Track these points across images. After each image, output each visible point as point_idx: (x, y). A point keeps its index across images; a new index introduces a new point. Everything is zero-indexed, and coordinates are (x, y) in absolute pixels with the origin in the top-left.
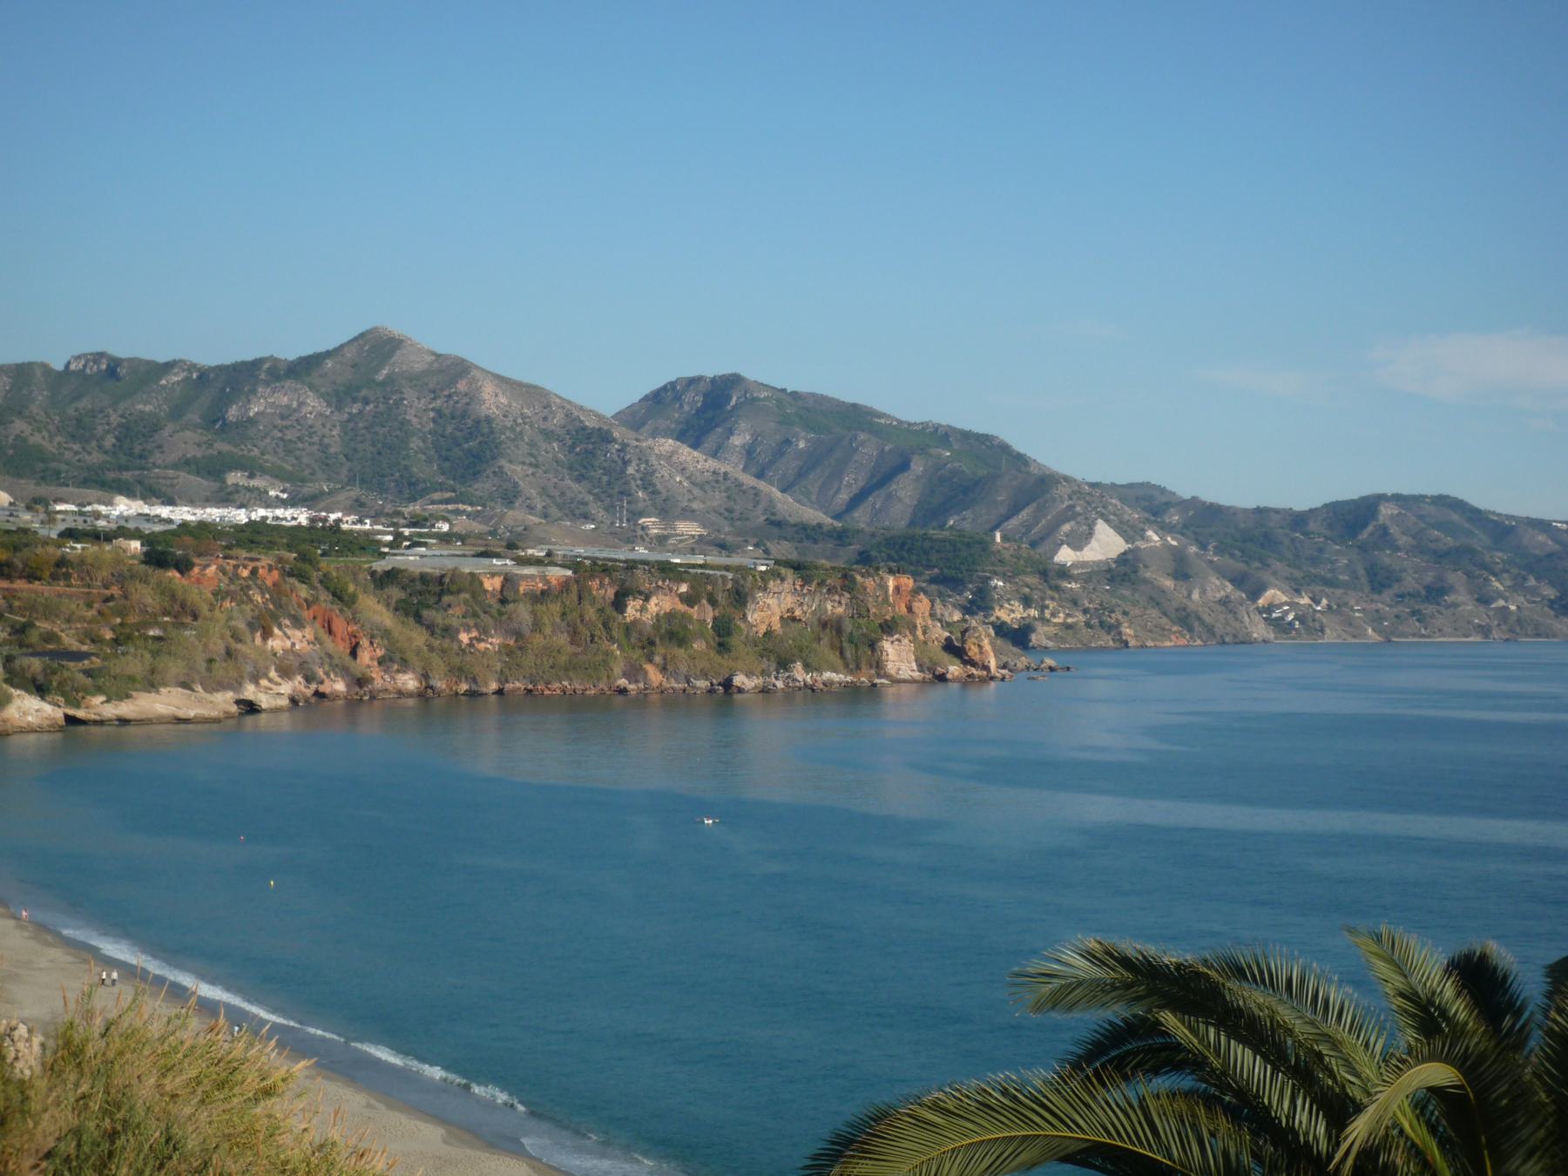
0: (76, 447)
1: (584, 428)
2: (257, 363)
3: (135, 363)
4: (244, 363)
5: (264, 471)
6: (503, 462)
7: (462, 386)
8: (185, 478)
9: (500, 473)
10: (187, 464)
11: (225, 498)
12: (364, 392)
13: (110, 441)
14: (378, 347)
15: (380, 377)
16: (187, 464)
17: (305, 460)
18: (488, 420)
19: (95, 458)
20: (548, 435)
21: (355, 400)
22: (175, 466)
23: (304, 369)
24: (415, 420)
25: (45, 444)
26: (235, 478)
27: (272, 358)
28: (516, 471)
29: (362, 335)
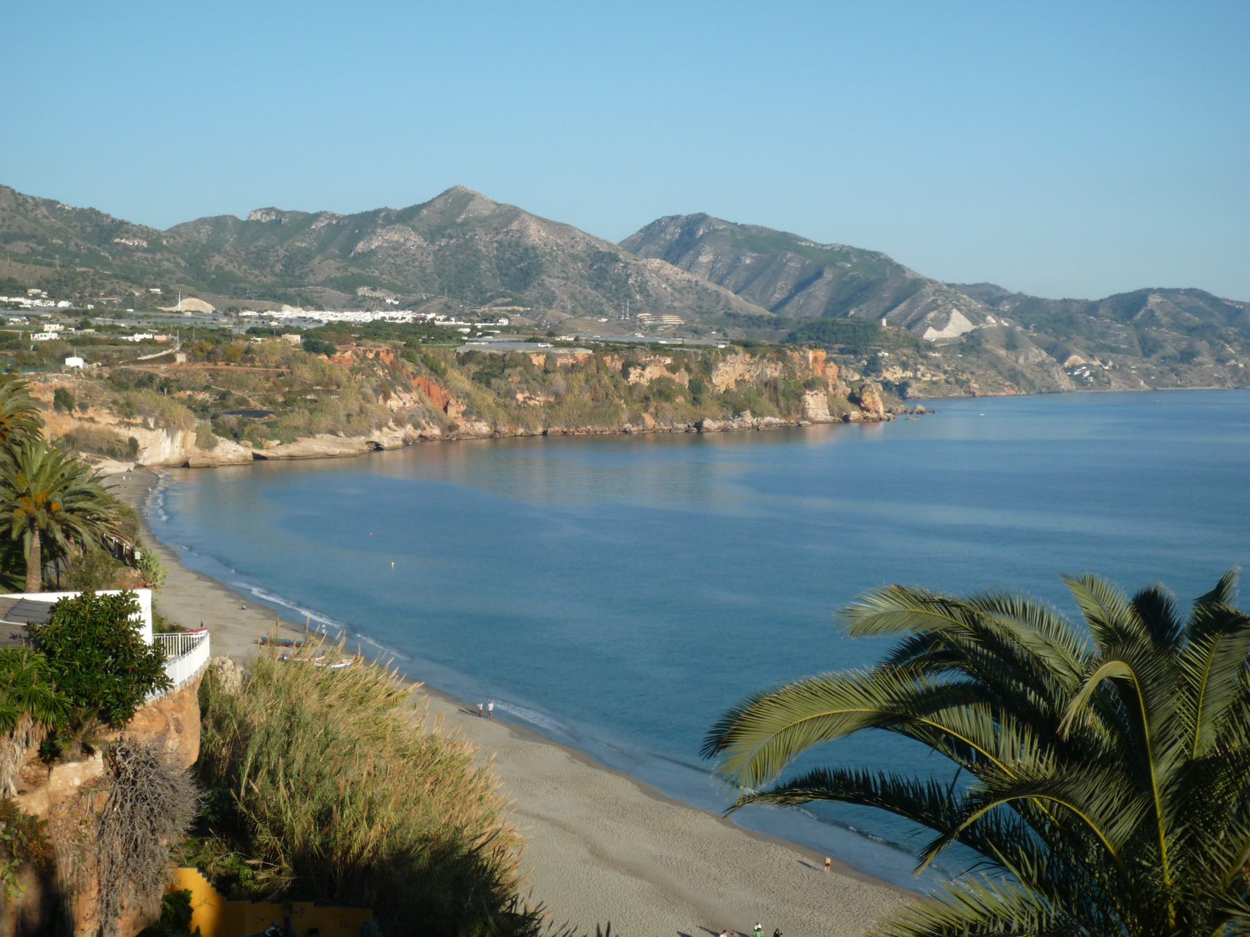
0: (256, 272)
1: (599, 252)
2: (376, 213)
3: (294, 214)
4: (367, 213)
5: (382, 286)
6: (544, 277)
7: (515, 226)
8: (330, 293)
9: (542, 285)
10: (331, 282)
11: (357, 305)
12: (449, 231)
13: (279, 268)
14: (458, 199)
15: (460, 220)
16: (331, 282)
17: (410, 278)
18: (534, 248)
19: (269, 279)
20: (575, 258)
21: (443, 236)
22: (323, 284)
23: (407, 216)
24: (484, 249)
25: (236, 271)
26: (363, 291)
27: (386, 209)
28: (553, 283)
29: (447, 192)
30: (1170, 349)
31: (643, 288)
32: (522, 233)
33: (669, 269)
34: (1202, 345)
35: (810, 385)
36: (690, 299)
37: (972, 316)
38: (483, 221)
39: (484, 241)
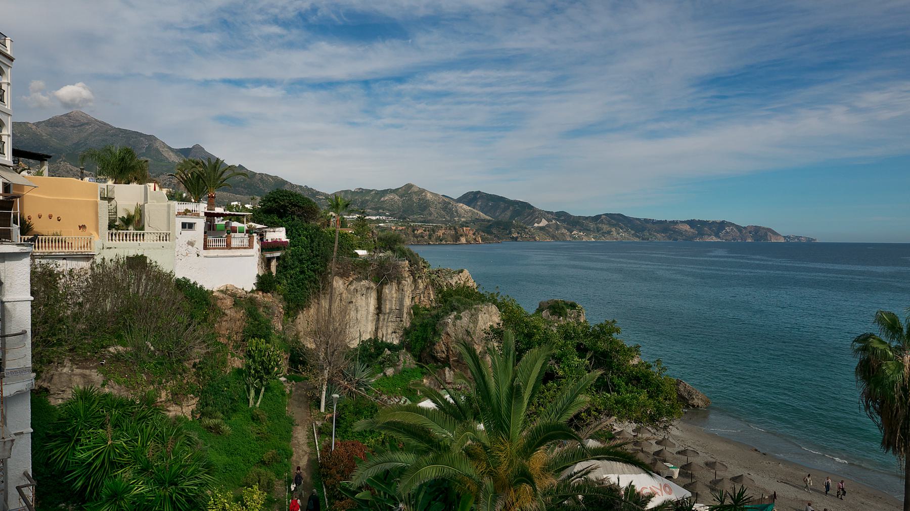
28: (432, 210)
30: (604, 230)
31: (456, 212)
32: (425, 196)
33: (465, 206)
34: (613, 229)
35: (461, 235)
36: (470, 214)
37: (548, 220)
38: (415, 193)
39: (415, 198)
